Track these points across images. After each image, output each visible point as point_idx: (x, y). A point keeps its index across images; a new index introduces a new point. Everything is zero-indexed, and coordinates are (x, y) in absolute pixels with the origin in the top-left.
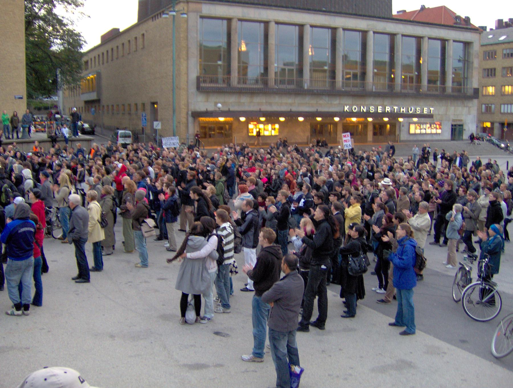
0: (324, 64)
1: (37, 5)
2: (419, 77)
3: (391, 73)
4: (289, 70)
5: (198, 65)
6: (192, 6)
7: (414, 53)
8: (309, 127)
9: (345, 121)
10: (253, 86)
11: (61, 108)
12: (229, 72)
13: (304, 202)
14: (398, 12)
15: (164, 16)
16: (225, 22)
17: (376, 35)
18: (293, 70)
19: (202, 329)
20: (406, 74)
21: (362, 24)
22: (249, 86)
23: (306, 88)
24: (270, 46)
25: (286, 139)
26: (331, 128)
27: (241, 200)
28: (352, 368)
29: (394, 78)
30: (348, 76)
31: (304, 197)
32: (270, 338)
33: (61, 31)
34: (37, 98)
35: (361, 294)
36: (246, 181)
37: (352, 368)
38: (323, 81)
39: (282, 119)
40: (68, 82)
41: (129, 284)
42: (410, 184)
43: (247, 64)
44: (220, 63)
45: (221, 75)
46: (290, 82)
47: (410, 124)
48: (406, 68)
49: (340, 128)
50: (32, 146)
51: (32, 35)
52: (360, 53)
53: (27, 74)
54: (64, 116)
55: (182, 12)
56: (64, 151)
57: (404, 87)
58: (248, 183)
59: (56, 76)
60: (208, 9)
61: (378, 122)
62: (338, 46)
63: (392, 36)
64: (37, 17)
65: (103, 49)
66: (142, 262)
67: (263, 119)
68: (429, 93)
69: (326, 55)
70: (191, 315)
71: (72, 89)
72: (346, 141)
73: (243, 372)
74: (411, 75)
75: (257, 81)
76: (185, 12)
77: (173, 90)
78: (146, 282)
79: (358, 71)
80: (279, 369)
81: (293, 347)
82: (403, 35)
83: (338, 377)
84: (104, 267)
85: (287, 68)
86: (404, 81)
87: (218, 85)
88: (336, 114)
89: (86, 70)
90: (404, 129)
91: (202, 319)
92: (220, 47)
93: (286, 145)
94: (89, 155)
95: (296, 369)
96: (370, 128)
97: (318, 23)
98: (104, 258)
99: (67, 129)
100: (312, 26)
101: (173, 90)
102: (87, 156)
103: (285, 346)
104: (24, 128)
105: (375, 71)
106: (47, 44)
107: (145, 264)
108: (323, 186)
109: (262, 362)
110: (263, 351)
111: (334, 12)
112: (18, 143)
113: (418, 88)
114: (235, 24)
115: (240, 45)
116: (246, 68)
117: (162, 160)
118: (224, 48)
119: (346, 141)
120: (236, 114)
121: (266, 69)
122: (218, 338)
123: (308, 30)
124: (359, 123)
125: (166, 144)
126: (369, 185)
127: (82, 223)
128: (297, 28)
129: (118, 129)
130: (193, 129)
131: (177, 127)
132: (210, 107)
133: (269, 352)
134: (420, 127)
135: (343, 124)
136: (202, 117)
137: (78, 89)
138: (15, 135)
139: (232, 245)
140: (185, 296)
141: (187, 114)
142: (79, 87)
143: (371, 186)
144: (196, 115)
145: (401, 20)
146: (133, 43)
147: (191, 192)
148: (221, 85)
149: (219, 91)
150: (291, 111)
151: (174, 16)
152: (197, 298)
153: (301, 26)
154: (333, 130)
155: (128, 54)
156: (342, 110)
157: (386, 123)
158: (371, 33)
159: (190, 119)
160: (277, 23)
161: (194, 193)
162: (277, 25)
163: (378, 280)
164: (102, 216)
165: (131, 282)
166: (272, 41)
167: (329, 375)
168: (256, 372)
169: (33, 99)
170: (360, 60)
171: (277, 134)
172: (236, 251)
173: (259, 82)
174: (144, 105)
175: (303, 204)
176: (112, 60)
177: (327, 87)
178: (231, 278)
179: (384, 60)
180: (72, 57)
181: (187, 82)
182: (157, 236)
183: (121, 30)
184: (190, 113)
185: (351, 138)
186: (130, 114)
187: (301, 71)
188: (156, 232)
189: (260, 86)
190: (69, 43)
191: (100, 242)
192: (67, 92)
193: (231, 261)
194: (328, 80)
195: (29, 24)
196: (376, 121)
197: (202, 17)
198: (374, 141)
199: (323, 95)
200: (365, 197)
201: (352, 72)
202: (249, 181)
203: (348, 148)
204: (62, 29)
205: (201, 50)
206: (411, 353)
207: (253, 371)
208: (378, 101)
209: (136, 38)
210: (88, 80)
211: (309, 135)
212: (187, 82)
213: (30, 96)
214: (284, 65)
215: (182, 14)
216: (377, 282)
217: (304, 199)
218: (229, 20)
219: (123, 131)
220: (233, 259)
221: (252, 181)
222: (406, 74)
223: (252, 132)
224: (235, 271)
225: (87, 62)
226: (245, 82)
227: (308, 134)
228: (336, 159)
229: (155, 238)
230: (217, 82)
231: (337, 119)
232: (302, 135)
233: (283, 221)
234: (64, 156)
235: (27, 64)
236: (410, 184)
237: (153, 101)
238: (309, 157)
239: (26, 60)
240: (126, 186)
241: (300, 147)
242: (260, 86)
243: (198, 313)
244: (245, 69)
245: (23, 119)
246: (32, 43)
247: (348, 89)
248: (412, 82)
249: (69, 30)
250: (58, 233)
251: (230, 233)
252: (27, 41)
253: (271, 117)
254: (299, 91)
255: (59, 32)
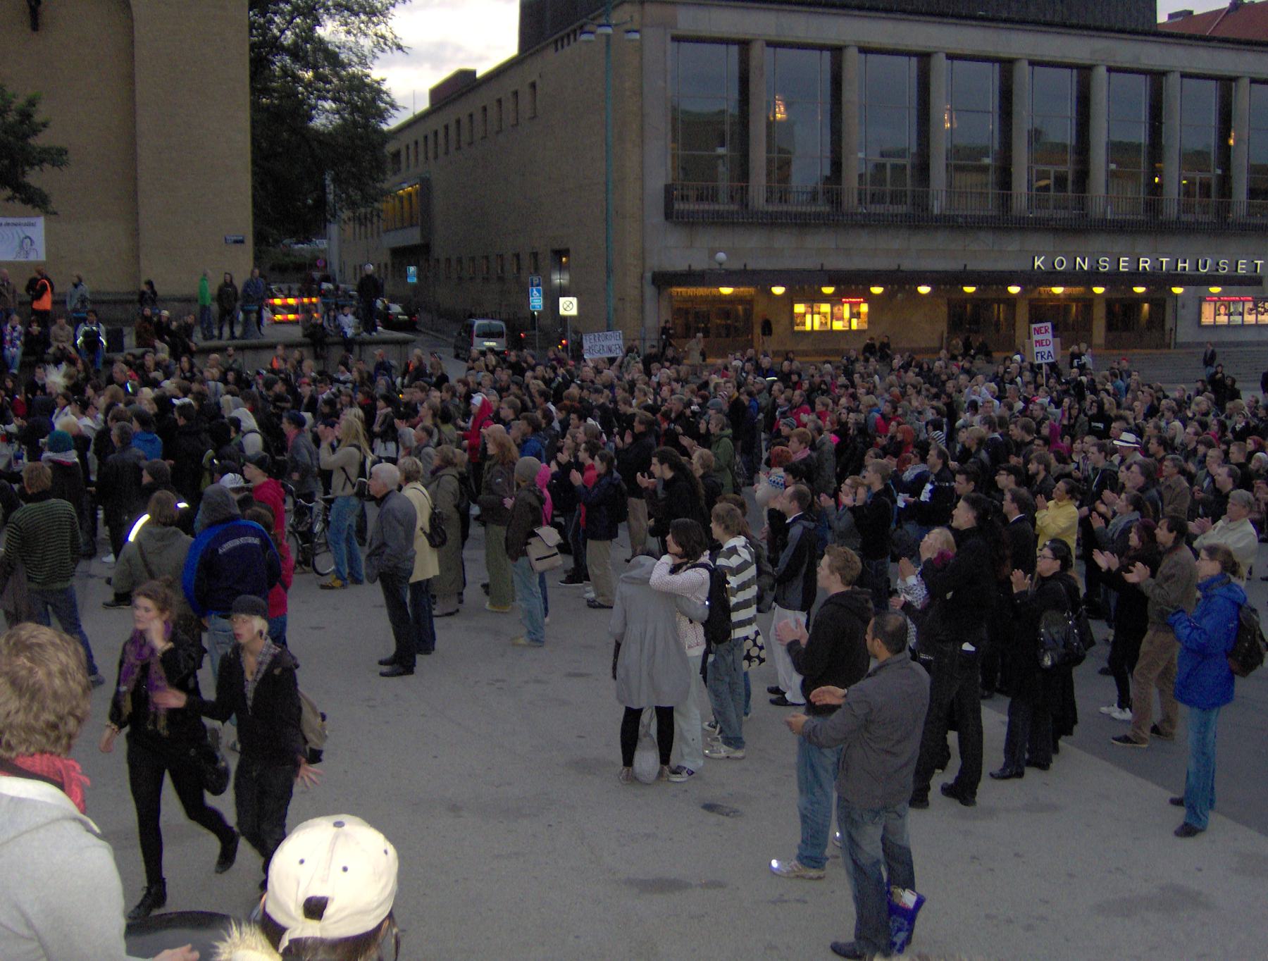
0: (984, 152)
1: (277, 19)
2: (1225, 182)
3: (1154, 172)
4: (894, 167)
5: (669, 157)
6: (652, 10)
7: (1213, 119)
8: (945, 309)
9: (1035, 295)
10: (804, 209)
11: (336, 267)
12: (744, 174)
13: (931, 491)
14: (1171, 16)
15: (585, 37)
16: (734, 50)
17: (1113, 75)
18: (905, 166)
19: (675, 796)
20: (1191, 175)
21: (1077, 48)
22: (794, 209)
23: (936, 211)
24: (846, 107)
25: (886, 340)
26: (1000, 311)
27: (771, 489)
28: (1047, 902)
29: (1160, 186)
30: (1043, 183)
31: (932, 478)
32: (839, 820)
33: (335, 80)
34: (277, 242)
35: (1065, 721)
36: (788, 438)
37: (1047, 902)
38: (981, 194)
39: (877, 290)
40: (353, 205)
41: (498, 684)
42: (1201, 449)
43: (789, 152)
44: (721, 151)
45: (724, 179)
46: (896, 198)
47: (1201, 300)
48: (1193, 159)
49: (1022, 312)
50: (267, 356)
51: (266, 91)
52: (1074, 121)
53: (254, 187)
54: (342, 286)
55: (628, 27)
56: (342, 368)
57: (1187, 209)
58: (794, 444)
59: (324, 187)
60: (689, 20)
61: (1120, 296)
62: (1016, 108)
63: (1157, 77)
64: (276, 46)
65: (437, 123)
66: (529, 632)
67: (828, 290)
68: (1253, 221)
69: (986, 130)
70: (647, 759)
71: (362, 221)
72: (1040, 343)
73: (774, 902)
74: (1206, 175)
75: (814, 197)
76: (636, 28)
77: (606, 220)
78: (538, 681)
79: (1069, 168)
80: (860, 900)
81: (900, 843)
82: (1184, 75)
83: (1010, 921)
84: (438, 644)
85: (889, 162)
86: (1187, 192)
87: (717, 207)
88: (1012, 278)
89: (395, 173)
90: (1186, 314)
91: (677, 771)
92: (722, 112)
93: (888, 356)
94: (403, 378)
95: (908, 899)
96: (1099, 313)
97: (968, 49)
98: (437, 623)
99: (351, 317)
100: (951, 57)
101: (606, 220)
102: (399, 380)
103: (878, 838)
104: (247, 313)
105: (1113, 166)
106: (298, 112)
107: (536, 639)
108: (978, 450)
109: (819, 878)
110: (822, 853)
111: (1005, 21)
112: (239, 349)
113: (1224, 208)
114: (758, 53)
115: (771, 106)
116: (788, 163)
117: (581, 388)
118: (732, 115)
119: (1040, 343)
120: (763, 279)
121: (837, 165)
122: (713, 818)
123: (940, 65)
124: (1068, 298)
125: (590, 350)
126: (1094, 449)
127: (402, 534)
128: (914, 60)
129: (471, 316)
130: (656, 316)
131: (615, 310)
132: (699, 262)
133: (837, 857)
134: (1227, 308)
135: (1031, 301)
136: (679, 285)
137: (375, 219)
138: (226, 330)
139: (752, 591)
140: (632, 717)
141: (642, 277)
142: (379, 216)
143: (1100, 451)
144: (663, 280)
145: (1181, 37)
146: (508, 105)
147: (655, 460)
148: (723, 206)
149: (721, 221)
150: (899, 270)
151: (608, 36)
152: (665, 716)
153: (924, 57)
154: (1006, 319)
155: (497, 133)
156: (1028, 267)
157: (1140, 299)
158: (1102, 71)
159: (650, 291)
160: (864, 50)
161: (662, 463)
162: (863, 56)
163: (1115, 688)
164: (435, 519)
165: (503, 681)
166: (851, 93)
167: (987, 916)
168: (805, 902)
169: (268, 244)
170: (1074, 142)
171: (865, 326)
172: (762, 607)
173: (820, 196)
174: (535, 255)
175: (928, 495)
176: (459, 148)
177: (990, 208)
178: (746, 674)
179: (1135, 140)
180: (361, 139)
181: (642, 200)
182: (566, 572)
183: (479, 75)
184: (648, 275)
185: (1054, 336)
186: (501, 279)
187: (923, 169)
188: (563, 562)
189: (823, 208)
190: (355, 109)
191: (428, 580)
192: (349, 228)
193: (749, 631)
194: (992, 191)
195: (259, 65)
196: (1115, 295)
197: (677, 39)
198: (1110, 344)
199: (980, 228)
200: (1086, 479)
201: (1052, 170)
202: (795, 439)
203: (1044, 361)
204: (337, 75)
205: (674, 120)
206: (1200, 870)
207: (798, 901)
208: (1121, 243)
209: (516, 94)
210: (401, 198)
211: (945, 329)
212: (642, 200)
213: (260, 238)
214: (882, 155)
215: (629, 32)
216: (1114, 693)
217: (932, 483)
218: (744, 45)
219: (486, 322)
220: (754, 627)
221: (802, 439)
222: (1191, 175)
223: (804, 324)
224: (758, 657)
225: (397, 155)
226: (783, 199)
227: (942, 326)
228: (1008, 386)
229: (564, 577)
230: (714, 198)
231: (1014, 290)
232: (927, 330)
233: (878, 533)
234: (342, 378)
235: (254, 162)
236: (1201, 449)
237: (557, 247)
238: (944, 383)
239: (253, 152)
240: (492, 449)
241: (924, 359)
242: (823, 208)
243: (665, 758)
244: (785, 164)
245: (245, 291)
246: (267, 109)
247: (1044, 214)
248: (1209, 196)
249: (354, 76)
250: (325, 562)
251: (746, 561)
252: (256, 107)
253: (850, 284)
254: (920, 220)
255: (330, 82)
